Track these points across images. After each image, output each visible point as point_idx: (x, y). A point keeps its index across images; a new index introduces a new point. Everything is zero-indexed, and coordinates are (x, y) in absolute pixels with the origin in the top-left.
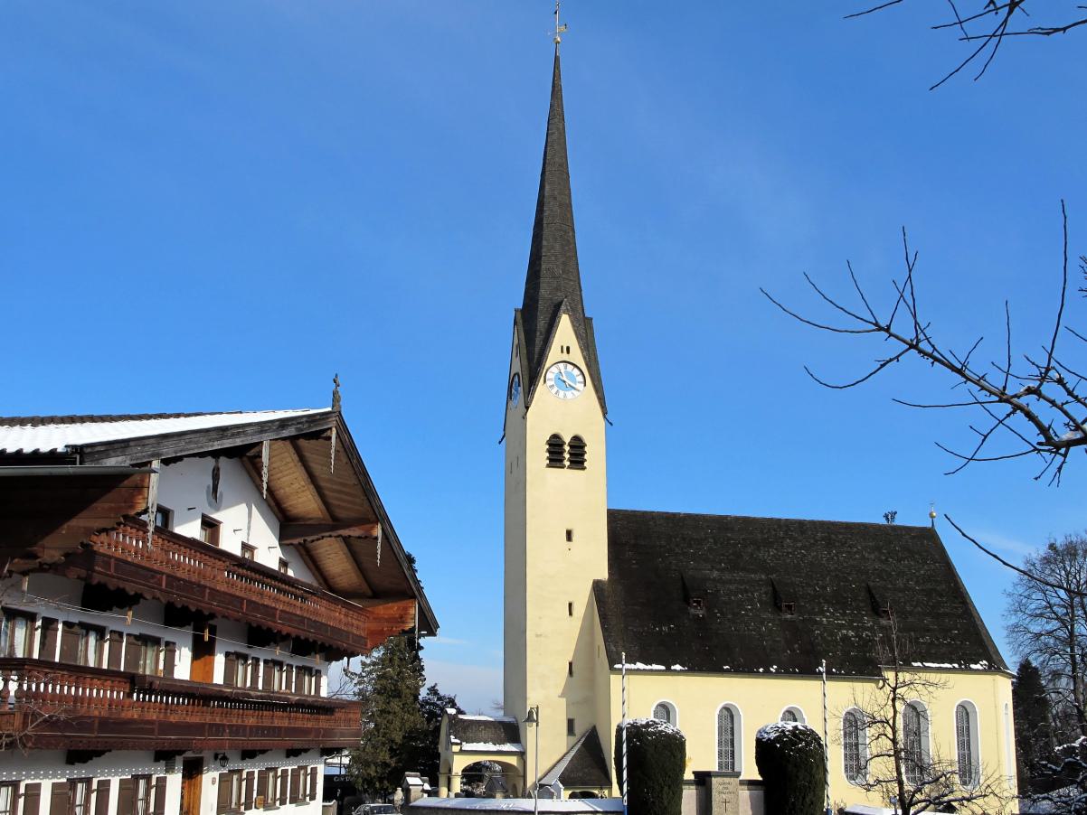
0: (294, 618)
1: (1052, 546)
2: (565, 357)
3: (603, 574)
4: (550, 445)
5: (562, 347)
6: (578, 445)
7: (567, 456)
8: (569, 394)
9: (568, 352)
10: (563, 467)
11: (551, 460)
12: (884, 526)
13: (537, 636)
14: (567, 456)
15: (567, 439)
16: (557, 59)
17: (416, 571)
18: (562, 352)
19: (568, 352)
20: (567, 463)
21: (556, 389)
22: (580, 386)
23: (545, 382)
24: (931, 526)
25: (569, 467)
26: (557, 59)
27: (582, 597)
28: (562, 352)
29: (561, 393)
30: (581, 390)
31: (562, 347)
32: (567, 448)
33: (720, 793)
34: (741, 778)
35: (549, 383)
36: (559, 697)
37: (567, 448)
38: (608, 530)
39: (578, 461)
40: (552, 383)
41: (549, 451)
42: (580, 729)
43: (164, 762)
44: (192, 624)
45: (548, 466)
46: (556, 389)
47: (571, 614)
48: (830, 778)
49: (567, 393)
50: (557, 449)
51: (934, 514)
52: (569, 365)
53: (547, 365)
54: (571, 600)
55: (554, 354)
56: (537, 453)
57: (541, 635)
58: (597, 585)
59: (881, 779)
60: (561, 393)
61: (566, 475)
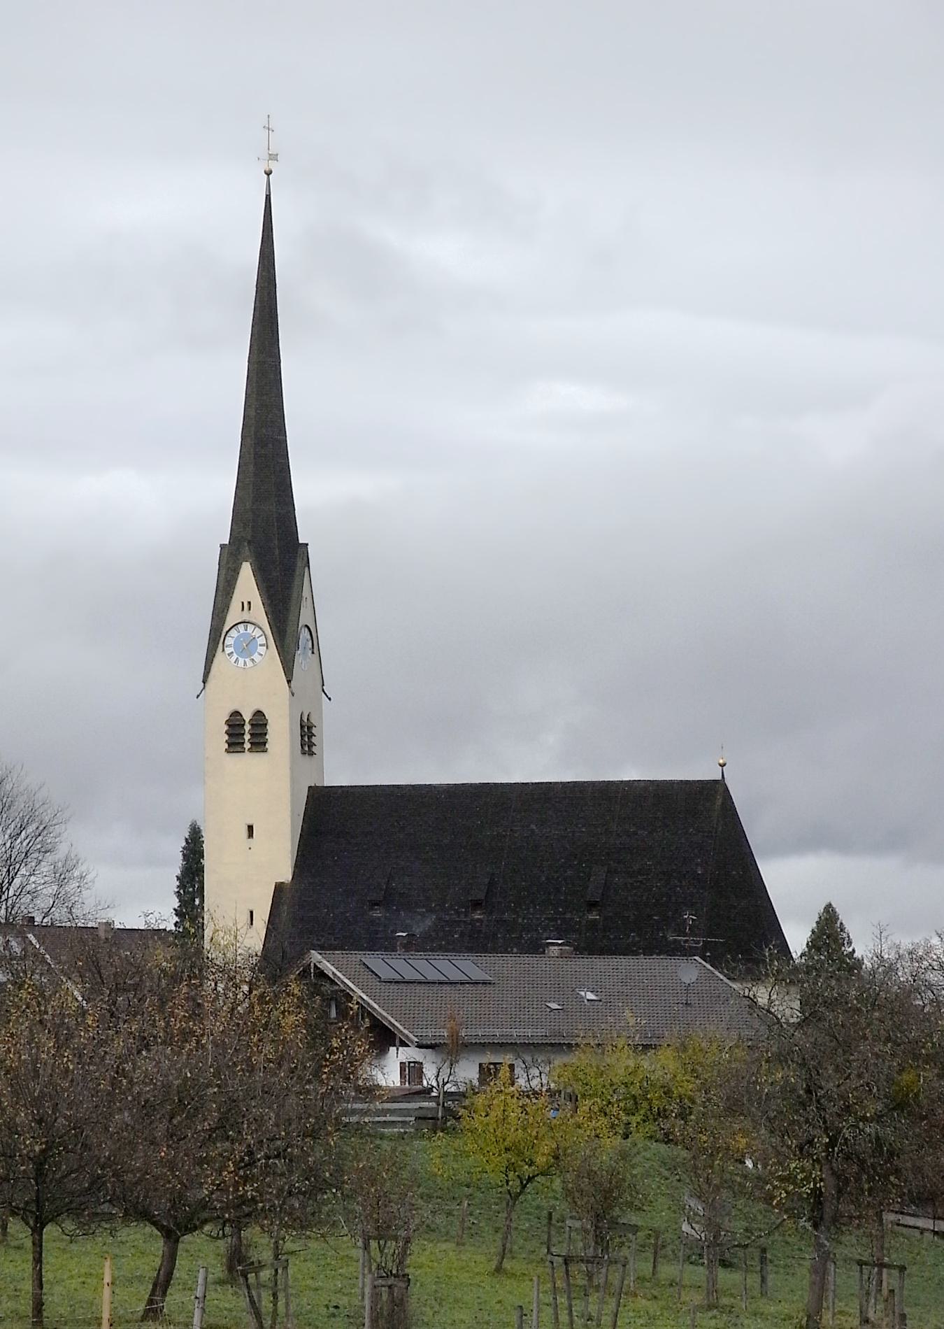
0: (200, 930)
1: (175, 909)
2: (246, 616)
3: (286, 875)
4: (229, 726)
5: (243, 603)
6: (260, 721)
7: (247, 737)
11: (230, 745)
14: (247, 737)
15: (247, 717)
17: (178, 878)
18: (249, 603)
20: (247, 746)
22: (262, 650)
23: (223, 650)
24: (720, 778)
28: (249, 603)
29: (241, 660)
31: (243, 603)
32: (247, 727)
34: (496, 1127)
35: (228, 650)
37: (247, 727)
38: (672, 783)
39: (259, 743)
40: (232, 649)
47: (252, 913)
50: (237, 731)
53: (226, 628)
56: (281, 734)
58: (279, 888)
59: (494, 1264)
60: (241, 660)
61: (248, 761)
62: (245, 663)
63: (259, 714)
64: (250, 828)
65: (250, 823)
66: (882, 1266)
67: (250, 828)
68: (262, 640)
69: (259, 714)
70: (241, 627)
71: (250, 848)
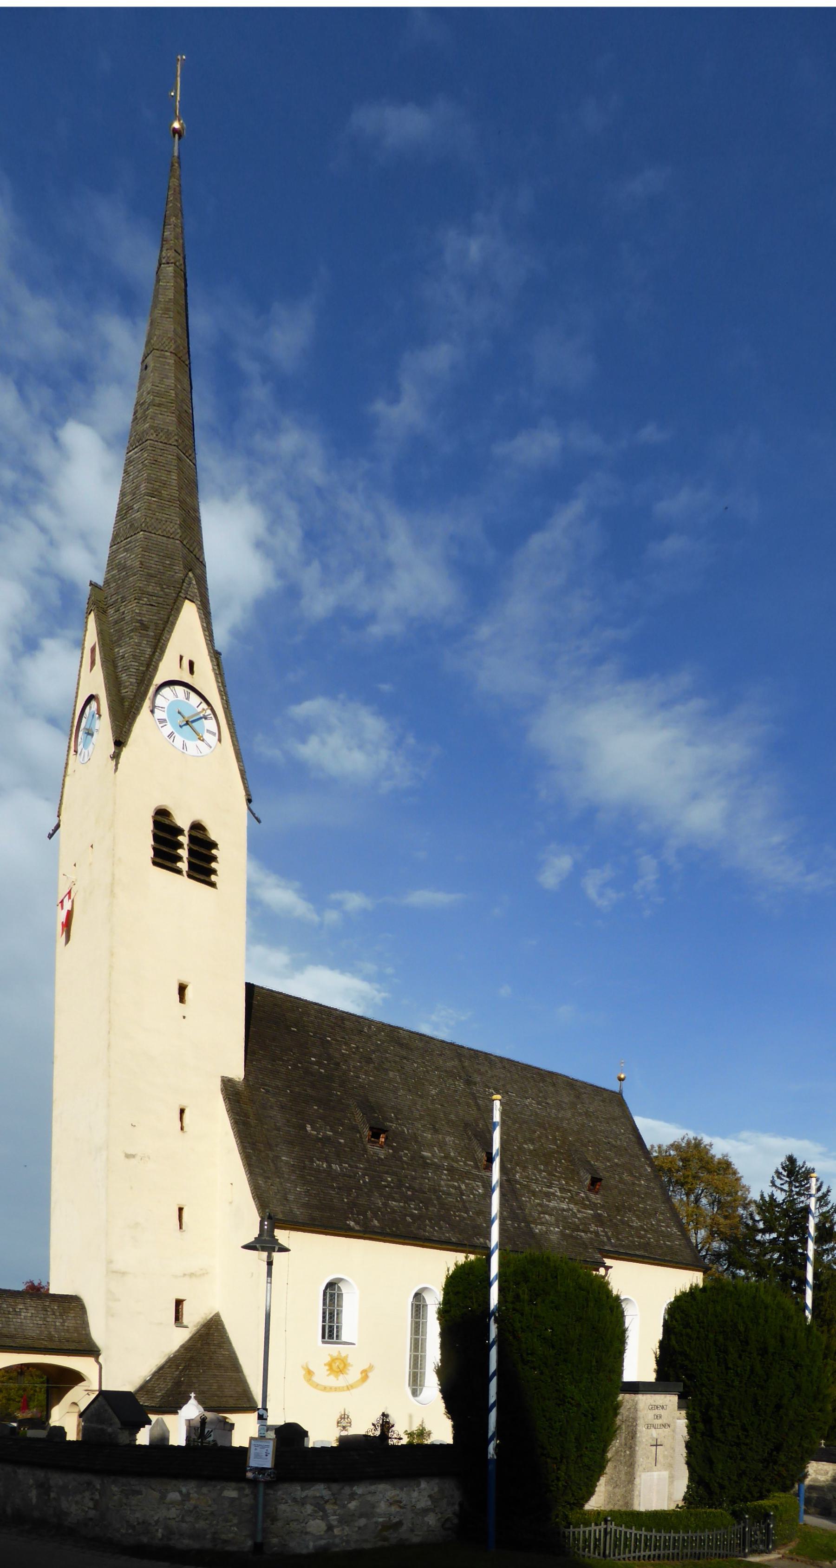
3: (237, 1072)
5: (181, 658)
7: (184, 853)
8: (193, 745)
9: (192, 671)
10: (179, 872)
12: (501, 1128)
13: (128, 1156)
15: (183, 821)
16: (269, 1274)
19: (192, 671)
20: (183, 866)
21: (168, 729)
22: (212, 740)
23: (152, 712)
25: (190, 876)
26: (269, 1274)
27: (127, 746)
28: (191, 664)
29: (179, 740)
30: (213, 746)
31: (181, 658)
32: (184, 839)
33: (649, 1426)
35: (158, 714)
36: (184, 1300)
41: (156, 838)
42: (194, 1317)
43: (127, 1432)
44: (193, 1395)
45: (155, 863)
46: (168, 729)
48: (657, 1334)
49: (189, 743)
51: (622, 1076)
52: (193, 695)
54: (184, 1103)
55: (167, 669)
57: (133, 1156)
62: (184, 746)
63: (197, 827)
64: (182, 989)
65: (184, 980)
66: (656, 1445)
67: (182, 989)
68: (210, 724)
69: (197, 827)
70: (180, 689)
71: (184, 1017)
